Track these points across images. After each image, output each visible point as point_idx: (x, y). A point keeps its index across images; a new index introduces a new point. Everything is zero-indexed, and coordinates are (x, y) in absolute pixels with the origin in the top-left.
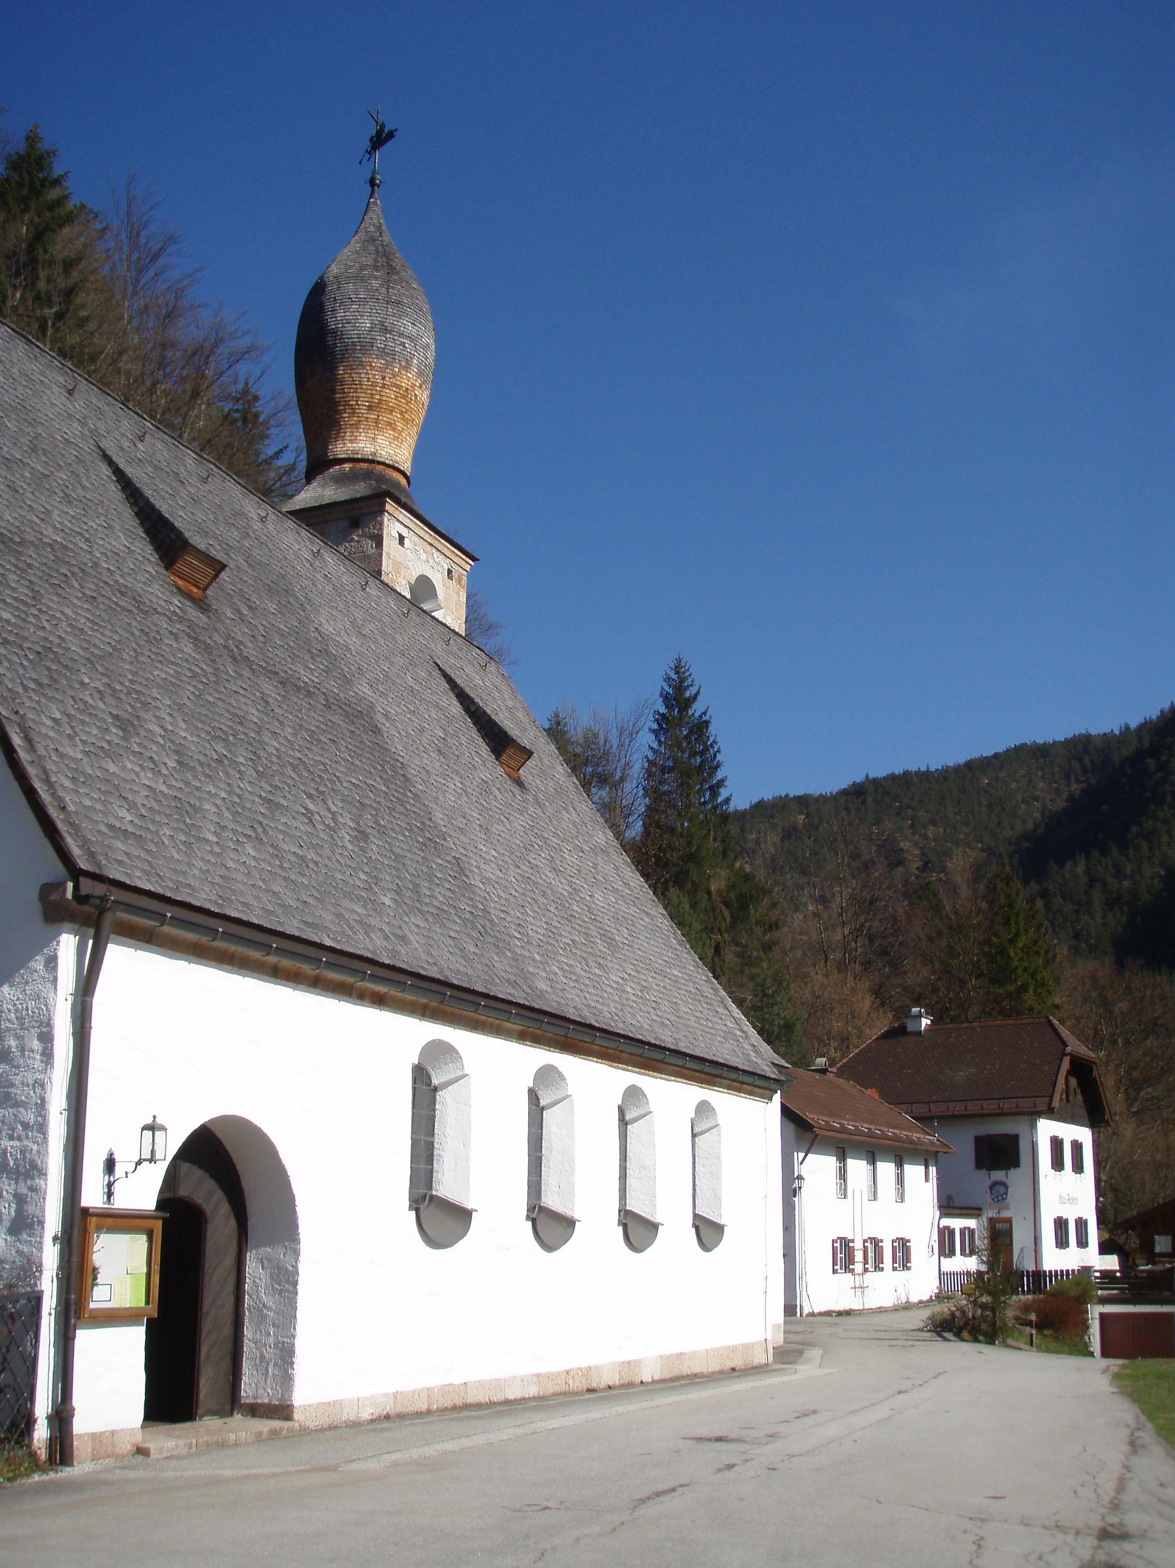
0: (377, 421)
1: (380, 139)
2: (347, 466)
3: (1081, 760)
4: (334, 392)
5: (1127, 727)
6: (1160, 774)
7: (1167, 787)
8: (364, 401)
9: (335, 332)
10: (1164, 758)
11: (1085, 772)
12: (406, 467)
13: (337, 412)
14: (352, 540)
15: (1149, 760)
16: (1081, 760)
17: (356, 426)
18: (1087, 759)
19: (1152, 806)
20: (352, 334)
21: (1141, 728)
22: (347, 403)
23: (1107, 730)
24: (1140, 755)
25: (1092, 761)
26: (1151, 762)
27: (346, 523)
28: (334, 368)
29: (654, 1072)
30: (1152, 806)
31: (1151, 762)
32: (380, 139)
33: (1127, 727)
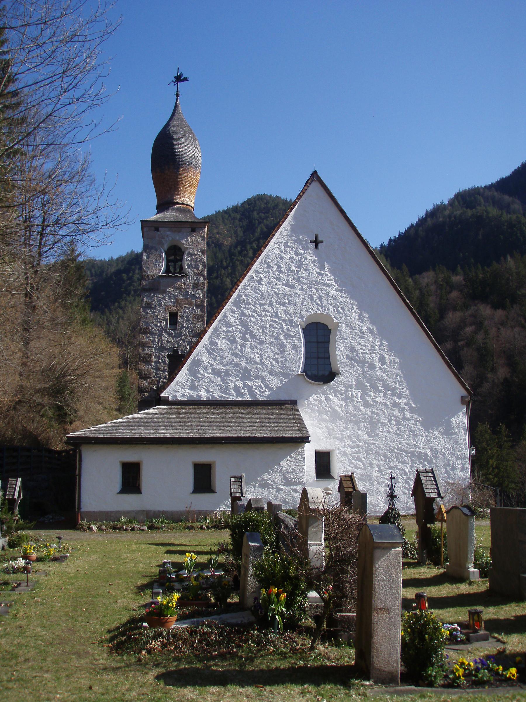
0: (191, 191)
1: (179, 79)
2: (182, 206)
3: (91, 271)
4: (177, 178)
5: (112, 258)
6: (129, 281)
7: (132, 287)
8: (188, 184)
9: (179, 156)
10: (131, 274)
11: (92, 276)
12: (193, 205)
13: (178, 185)
14: (193, 236)
15: (124, 275)
16: (91, 271)
17: (185, 191)
18: (93, 271)
19: (125, 295)
20: (186, 158)
21: (118, 259)
22: (182, 183)
23: (103, 259)
24: (118, 273)
25: (95, 272)
26: (125, 276)
27: (190, 229)
28: (178, 169)
29: (288, 437)
30: (125, 295)
31: (125, 276)
32: (179, 79)
33: (112, 258)
